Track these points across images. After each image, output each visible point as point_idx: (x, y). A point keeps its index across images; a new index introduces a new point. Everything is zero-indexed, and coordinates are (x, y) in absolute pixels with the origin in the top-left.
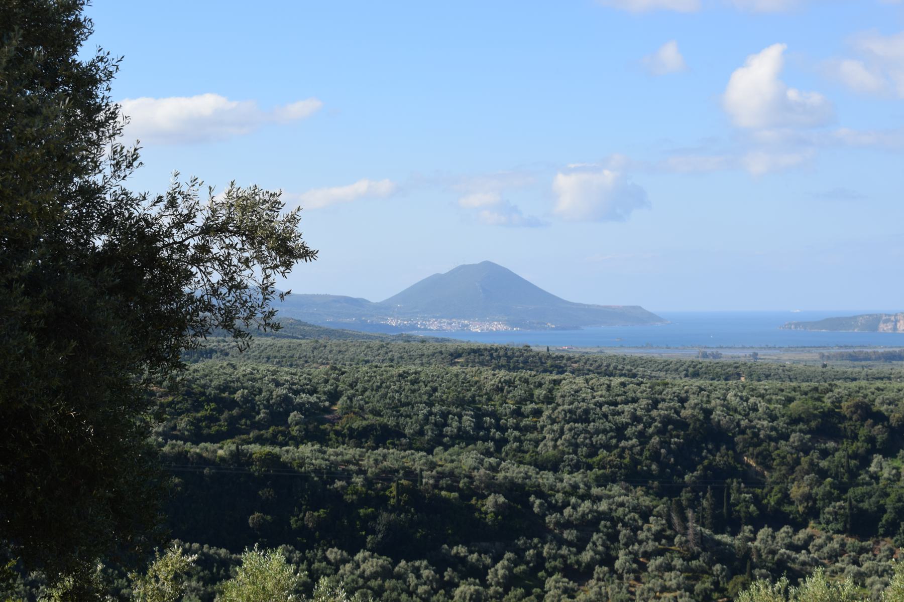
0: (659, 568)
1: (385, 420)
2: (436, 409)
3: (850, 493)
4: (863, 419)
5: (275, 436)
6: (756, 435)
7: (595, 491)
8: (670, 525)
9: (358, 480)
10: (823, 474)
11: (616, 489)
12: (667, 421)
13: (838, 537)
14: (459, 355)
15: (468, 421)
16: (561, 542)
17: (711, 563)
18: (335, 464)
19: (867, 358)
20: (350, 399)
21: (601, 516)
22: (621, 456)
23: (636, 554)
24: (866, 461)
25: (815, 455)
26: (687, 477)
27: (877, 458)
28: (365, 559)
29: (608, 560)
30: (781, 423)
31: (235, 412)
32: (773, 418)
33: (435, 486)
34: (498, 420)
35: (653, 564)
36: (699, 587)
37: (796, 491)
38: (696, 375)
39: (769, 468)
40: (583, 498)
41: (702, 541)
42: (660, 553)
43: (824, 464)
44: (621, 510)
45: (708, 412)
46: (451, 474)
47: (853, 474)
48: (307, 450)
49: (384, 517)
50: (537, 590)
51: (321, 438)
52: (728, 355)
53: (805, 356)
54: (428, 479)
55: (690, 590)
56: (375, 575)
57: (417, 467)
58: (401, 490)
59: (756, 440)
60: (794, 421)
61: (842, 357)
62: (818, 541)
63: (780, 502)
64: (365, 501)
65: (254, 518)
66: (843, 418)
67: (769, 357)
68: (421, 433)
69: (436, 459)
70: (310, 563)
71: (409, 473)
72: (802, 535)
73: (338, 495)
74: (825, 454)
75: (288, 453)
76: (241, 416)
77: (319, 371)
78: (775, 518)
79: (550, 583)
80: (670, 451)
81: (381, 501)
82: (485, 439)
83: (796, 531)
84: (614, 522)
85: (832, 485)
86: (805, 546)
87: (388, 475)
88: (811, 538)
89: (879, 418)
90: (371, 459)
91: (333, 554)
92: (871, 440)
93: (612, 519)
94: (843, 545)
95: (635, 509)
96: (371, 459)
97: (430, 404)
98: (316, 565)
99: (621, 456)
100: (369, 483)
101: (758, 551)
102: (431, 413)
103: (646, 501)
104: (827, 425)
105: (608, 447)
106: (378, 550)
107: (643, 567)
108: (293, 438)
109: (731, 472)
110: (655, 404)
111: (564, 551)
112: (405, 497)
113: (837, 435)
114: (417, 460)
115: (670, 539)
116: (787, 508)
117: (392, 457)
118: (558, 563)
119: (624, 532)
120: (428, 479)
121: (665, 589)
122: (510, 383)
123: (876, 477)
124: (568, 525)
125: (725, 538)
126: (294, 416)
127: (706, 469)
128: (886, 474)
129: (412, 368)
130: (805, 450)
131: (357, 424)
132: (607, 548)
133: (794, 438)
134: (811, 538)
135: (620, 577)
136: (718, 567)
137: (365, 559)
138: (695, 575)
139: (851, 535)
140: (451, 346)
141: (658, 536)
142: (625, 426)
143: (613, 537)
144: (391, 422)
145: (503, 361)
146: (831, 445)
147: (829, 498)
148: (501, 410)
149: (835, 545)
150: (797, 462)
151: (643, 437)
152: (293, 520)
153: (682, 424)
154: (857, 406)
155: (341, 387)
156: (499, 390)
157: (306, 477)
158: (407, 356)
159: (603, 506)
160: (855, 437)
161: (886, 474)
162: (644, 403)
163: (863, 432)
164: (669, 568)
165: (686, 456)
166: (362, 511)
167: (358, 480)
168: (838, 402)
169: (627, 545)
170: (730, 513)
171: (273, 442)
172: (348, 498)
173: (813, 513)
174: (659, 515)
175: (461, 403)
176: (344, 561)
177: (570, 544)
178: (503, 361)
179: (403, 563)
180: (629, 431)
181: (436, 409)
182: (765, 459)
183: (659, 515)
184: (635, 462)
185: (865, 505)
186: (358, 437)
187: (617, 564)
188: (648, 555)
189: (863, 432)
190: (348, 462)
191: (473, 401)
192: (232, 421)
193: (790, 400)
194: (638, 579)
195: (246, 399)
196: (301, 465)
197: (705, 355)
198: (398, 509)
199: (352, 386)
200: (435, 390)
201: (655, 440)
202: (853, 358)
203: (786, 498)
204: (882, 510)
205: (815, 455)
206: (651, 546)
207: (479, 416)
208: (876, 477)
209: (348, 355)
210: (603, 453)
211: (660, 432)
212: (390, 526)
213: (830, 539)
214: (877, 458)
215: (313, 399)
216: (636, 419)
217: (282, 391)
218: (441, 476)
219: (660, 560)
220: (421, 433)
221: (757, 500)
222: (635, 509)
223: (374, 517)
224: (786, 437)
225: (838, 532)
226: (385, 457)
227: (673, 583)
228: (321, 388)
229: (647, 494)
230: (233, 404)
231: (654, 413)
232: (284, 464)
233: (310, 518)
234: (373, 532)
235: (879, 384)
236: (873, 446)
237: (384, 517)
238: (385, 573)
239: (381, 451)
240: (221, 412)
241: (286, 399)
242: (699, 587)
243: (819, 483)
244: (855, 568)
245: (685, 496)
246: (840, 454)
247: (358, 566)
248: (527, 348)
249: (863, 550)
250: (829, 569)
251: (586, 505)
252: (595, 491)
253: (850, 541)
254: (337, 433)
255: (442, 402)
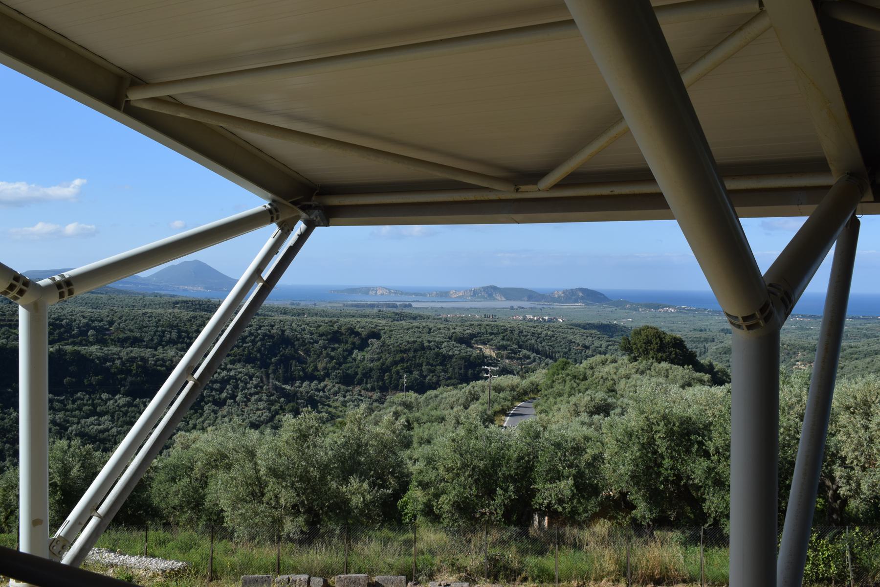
0: (256, 400)
1: (135, 334)
2: (160, 329)
3: (344, 366)
4: (350, 335)
5: (81, 341)
6: (304, 341)
7: (229, 366)
8: (262, 381)
9: (118, 362)
10: (332, 358)
11: (238, 365)
12: (265, 335)
13: (337, 386)
14: (177, 303)
15: (174, 335)
16: (212, 389)
17: (279, 398)
18: (108, 355)
19: (363, 306)
20: (119, 324)
21: (231, 378)
22: (244, 351)
23: (246, 394)
24: (351, 353)
25: (329, 350)
26: (273, 360)
27: (356, 351)
28: (120, 398)
29: (233, 397)
30: (315, 337)
31: (62, 330)
32: (312, 334)
33: (155, 365)
34: (188, 334)
35: (253, 398)
36: (273, 408)
37: (320, 366)
38: (285, 313)
39: (309, 356)
40: (223, 370)
41: (276, 388)
42: (257, 393)
43: (333, 354)
44: (240, 375)
45: (283, 331)
46: (163, 359)
47: (345, 358)
48: (94, 349)
49: (129, 379)
50: (200, 411)
51: (101, 342)
52: (304, 304)
53: (336, 305)
54: (151, 361)
55: (269, 409)
56: (124, 406)
57: (147, 356)
58: (138, 367)
59: (304, 343)
60: (321, 335)
61: (352, 305)
62: (329, 387)
63: (313, 370)
64: (121, 371)
65: (66, 380)
66: (342, 334)
67: (321, 306)
68: (152, 340)
69: (157, 353)
70: (93, 400)
71: (143, 359)
72: (322, 384)
73: (108, 369)
74: (333, 349)
75: (83, 350)
76: (65, 332)
77: (104, 312)
78: (311, 378)
79: (206, 408)
80: (265, 348)
81: (128, 372)
82: (182, 343)
83: (320, 383)
84: (237, 380)
85: (336, 363)
86: (323, 390)
87: (132, 360)
88: (326, 386)
89: (357, 334)
90: (125, 353)
91: (104, 396)
92: (353, 343)
93: (236, 379)
94: (339, 389)
95: (246, 374)
96: (125, 353)
97: (157, 327)
98: (96, 401)
99: (244, 351)
100: (123, 364)
101: (301, 393)
102: (157, 331)
103: (252, 371)
104: (335, 337)
105: (238, 347)
106: (126, 394)
107: (249, 400)
108: (90, 342)
109: (293, 357)
110: (260, 327)
111: (214, 393)
112: (140, 370)
113: (339, 342)
114: (148, 353)
115: (262, 388)
116: (316, 373)
117: (136, 351)
118: (210, 399)
119: (241, 385)
120: (151, 361)
121: (258, 409)
122: (195, 317)
123: (355, 360)
124: (216, 381)
125: (288, 387)
126: (90, 332)
127: (281, 356)
128: (359, 358)
129: (150, 310)
130: (325, 348)
131: (122, 336)
132: (233, 392)
133: (321, 342)
134: (326, 386)
135: (238, 405)
136: (282, 399)
137: (120, 398)
138: (272, 403)
139: (343, 384)
140: (174, 300)
141: (256, 387)
142: (246, 337)
143: (236, 387)
144: (138, 335)
145: (198, 306)
146: (336, 345)
147: (334, 368)
148: (190, 330)
149: (336, 389)
150: (321, 353)
151: (254, 342)
152: (85, 381)
153: (271, 337)
154: (348, 329)
155: (115, 318)
156: (189, 320)
157: (93, 361)
158: (153, 305)
159: (232, 373)
160: (347, 342)
161: (359, 358)
162: (254, 327)
163: (350, 340)
164: (260, 400)
165: (273, 350)
166: (119, 377)
167: (118, 362)
168: (340, 327)
169: (242, 390)
170: (291, 375)
171: (80, 344)
172: (113, 370)
173: (327, 375)
174: (257, 377)
175: (172, 326)
176: (110, 399)
177: (216, 390)
178: (198, 306)
179: (138, 400)
180: (247, 340)
181: (160, 329)
182: (307, 352)
183: (257, 377)
184: (250, 353)
185: (349, 372)
186: (122, 342)
187: (237, 399)
188: (251, 395)
189: (350, 340)
190: (114, 354)
191: (177, 325)
192: (60, 334)
193: (320, 326)
194: (246, 405)
195: (67, 324)
196: (91, 355)
197: (293, 304)
198: (136, 375)
199: (120, 318)
200: (159, 320)
201: (259, 344)
202: (357, 306)
203: (316, 369)
204: (356, 373)
205: (329, 350)
206: (253, 390)
207: (180, 332)
208: (355, 360)
209: (125, 302)
210: (236, 349)
211: (261, 340)
212: (132, 383)
213: (334, 386)
214: (356, 351)
215: (101, 324)
216: (251, 334)
217: (85, 321)
218: (158, 360)
219: (256, 397)
220: (152, 340)
221: (303, 370)
222: (246, 374)
223: (125, 379)
224: (317, 343)
225: (337, 383)
226: (132, 352)
227: (261, 407)
228: (105, 319)
229: (253, 367)
230: (62, 326)
231: (259, 331)
232: (83, 355)
233: (94, 379)
234: (124, 386)
235: (359, 319)
236: (354, 346)
237: (129, 379)
238: (129, 405)
239: (130, 349)
240: (55, 330)
241: (87, 325)
242: (273, 408)
243: (330, 362)
244: (343, 399)
245: (272, 368)
246: (340, 349)
247: (116, 401)
248: (209, 301)
249: (347, 391)
250: (220, 413)
251: (224, 373)
252: (229, 366)
253: (342, 387)
254: (112, 340)
255: (163, 326)
